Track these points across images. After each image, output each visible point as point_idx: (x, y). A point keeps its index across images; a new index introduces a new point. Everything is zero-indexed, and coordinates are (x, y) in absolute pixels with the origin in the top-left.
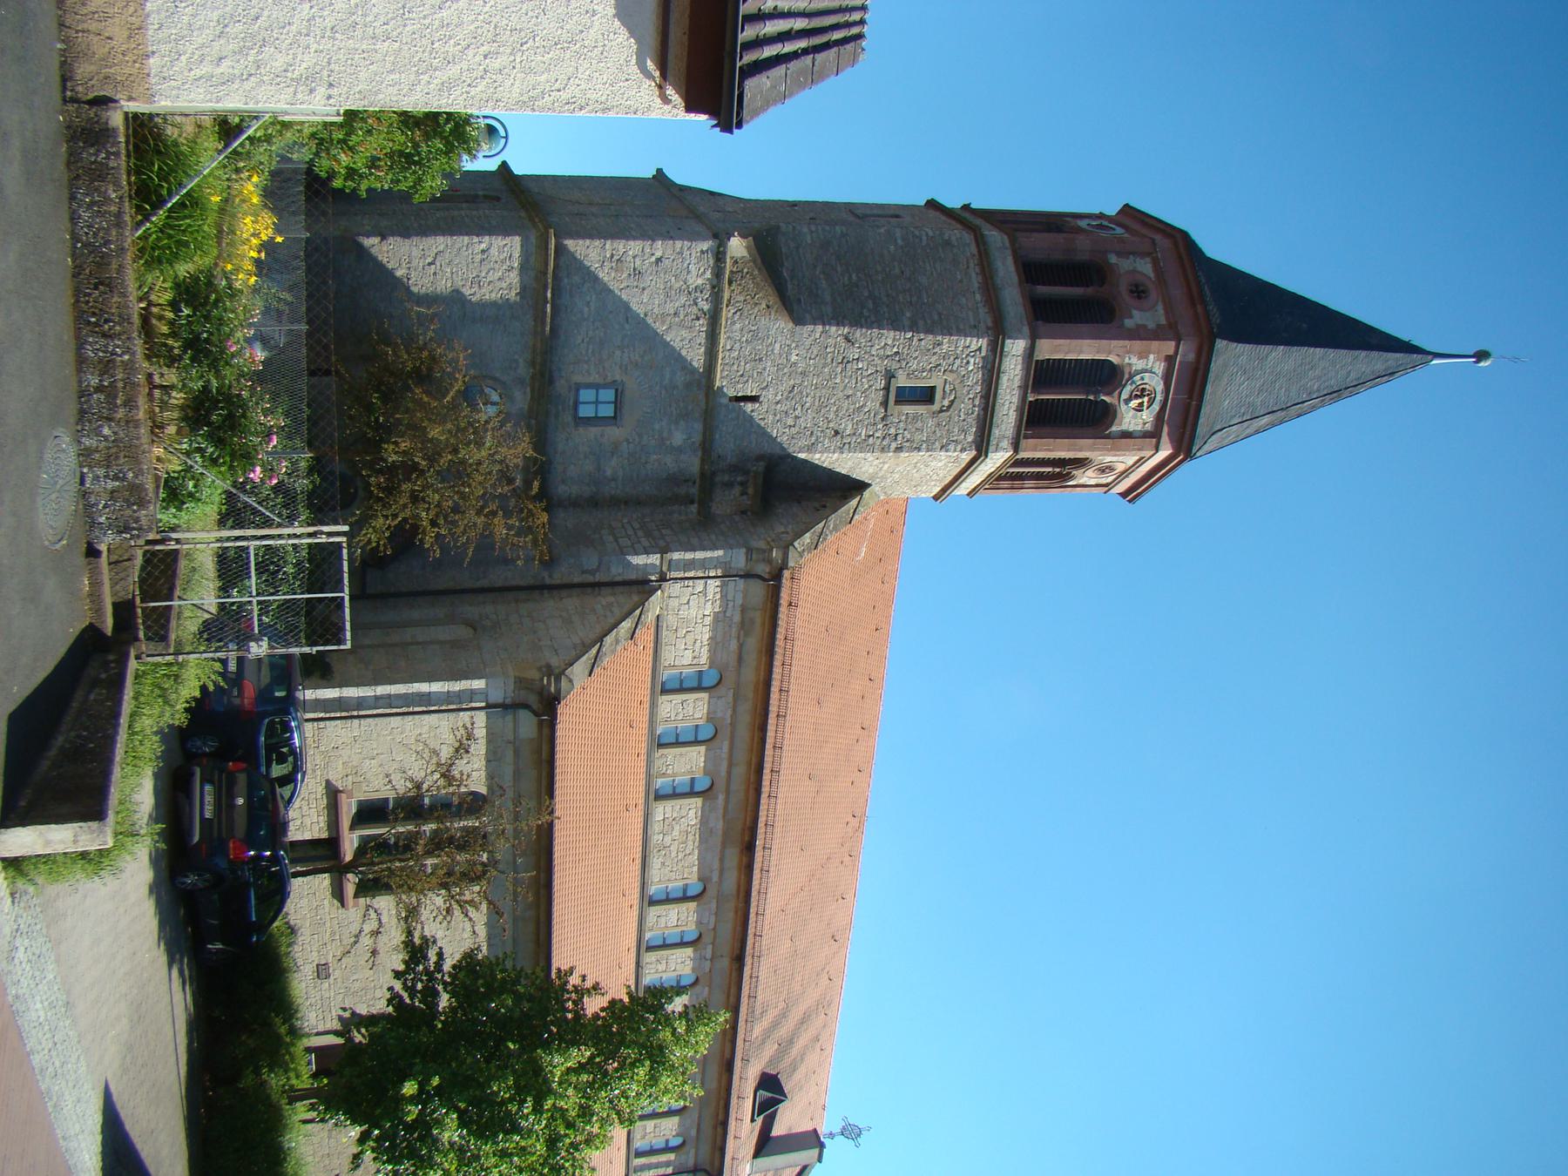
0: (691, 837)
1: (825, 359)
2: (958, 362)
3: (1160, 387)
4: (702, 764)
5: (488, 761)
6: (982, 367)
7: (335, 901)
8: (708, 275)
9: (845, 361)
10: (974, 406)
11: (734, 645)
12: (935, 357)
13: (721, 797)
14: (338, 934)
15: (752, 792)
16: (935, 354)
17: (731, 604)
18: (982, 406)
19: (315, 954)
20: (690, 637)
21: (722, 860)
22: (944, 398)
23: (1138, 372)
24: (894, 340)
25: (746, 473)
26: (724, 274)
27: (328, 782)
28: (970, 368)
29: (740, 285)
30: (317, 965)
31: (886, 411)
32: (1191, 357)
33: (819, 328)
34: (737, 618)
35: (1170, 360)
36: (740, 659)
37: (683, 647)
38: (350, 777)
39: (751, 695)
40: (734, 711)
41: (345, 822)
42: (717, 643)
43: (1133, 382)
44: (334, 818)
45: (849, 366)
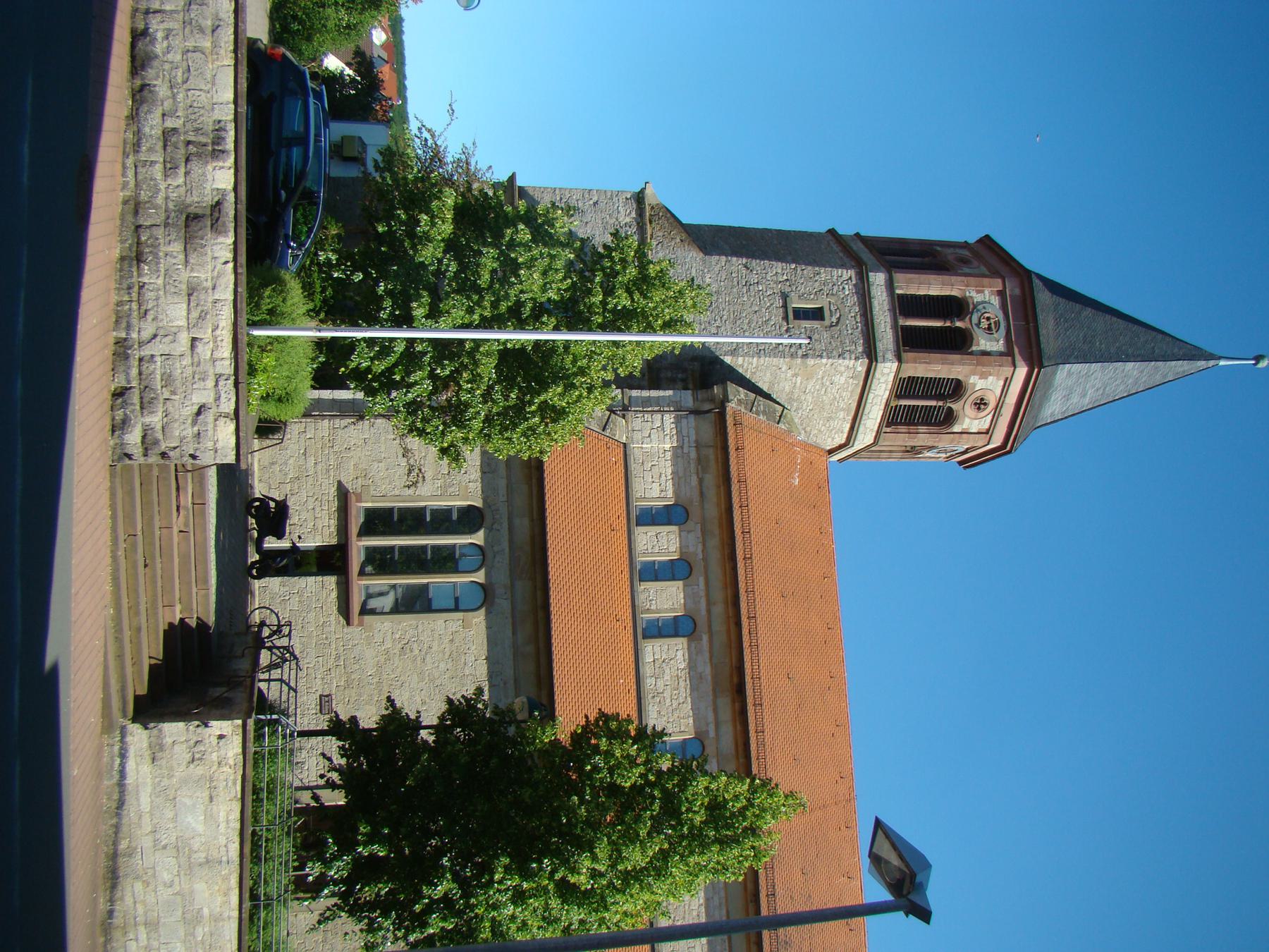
0: (682, 684)
1: (732, 281)
3: (1001, 317)
4: (682, 601)
5: (483, 473)
6: (856, 293)
7: (341, 618)
8: (634, 215)
9: (748, 284)
10: (857, 322)
11: (694, 481)
12: (817, 284)
13: (705, 638)
14: (342, 658)
15: (733, 627)
17: (686, 440)
18: (863, 323)
19: (319, 682)
20: (655, 470)
21: (715, 711)
22: (831, 316)
23: (979, 303)
24: (782, 269)
25: (685, 371)
27: (340, 483)
28: (847, 293)
29: (658, 224)
30: (321, 696)
31: (788, 324)
32: (1017, 291)
33: (723, 258)
34: (693, 455)
35: (1001, 294)
36: (702, 494)
37: (650, 480)
38: (360, 479)
39: (717, 531)
40: (704, 545)
41: (354, 529)
42: (679, 478)
43: (978, 310)
44: (344, 523)
45: (752, 287)
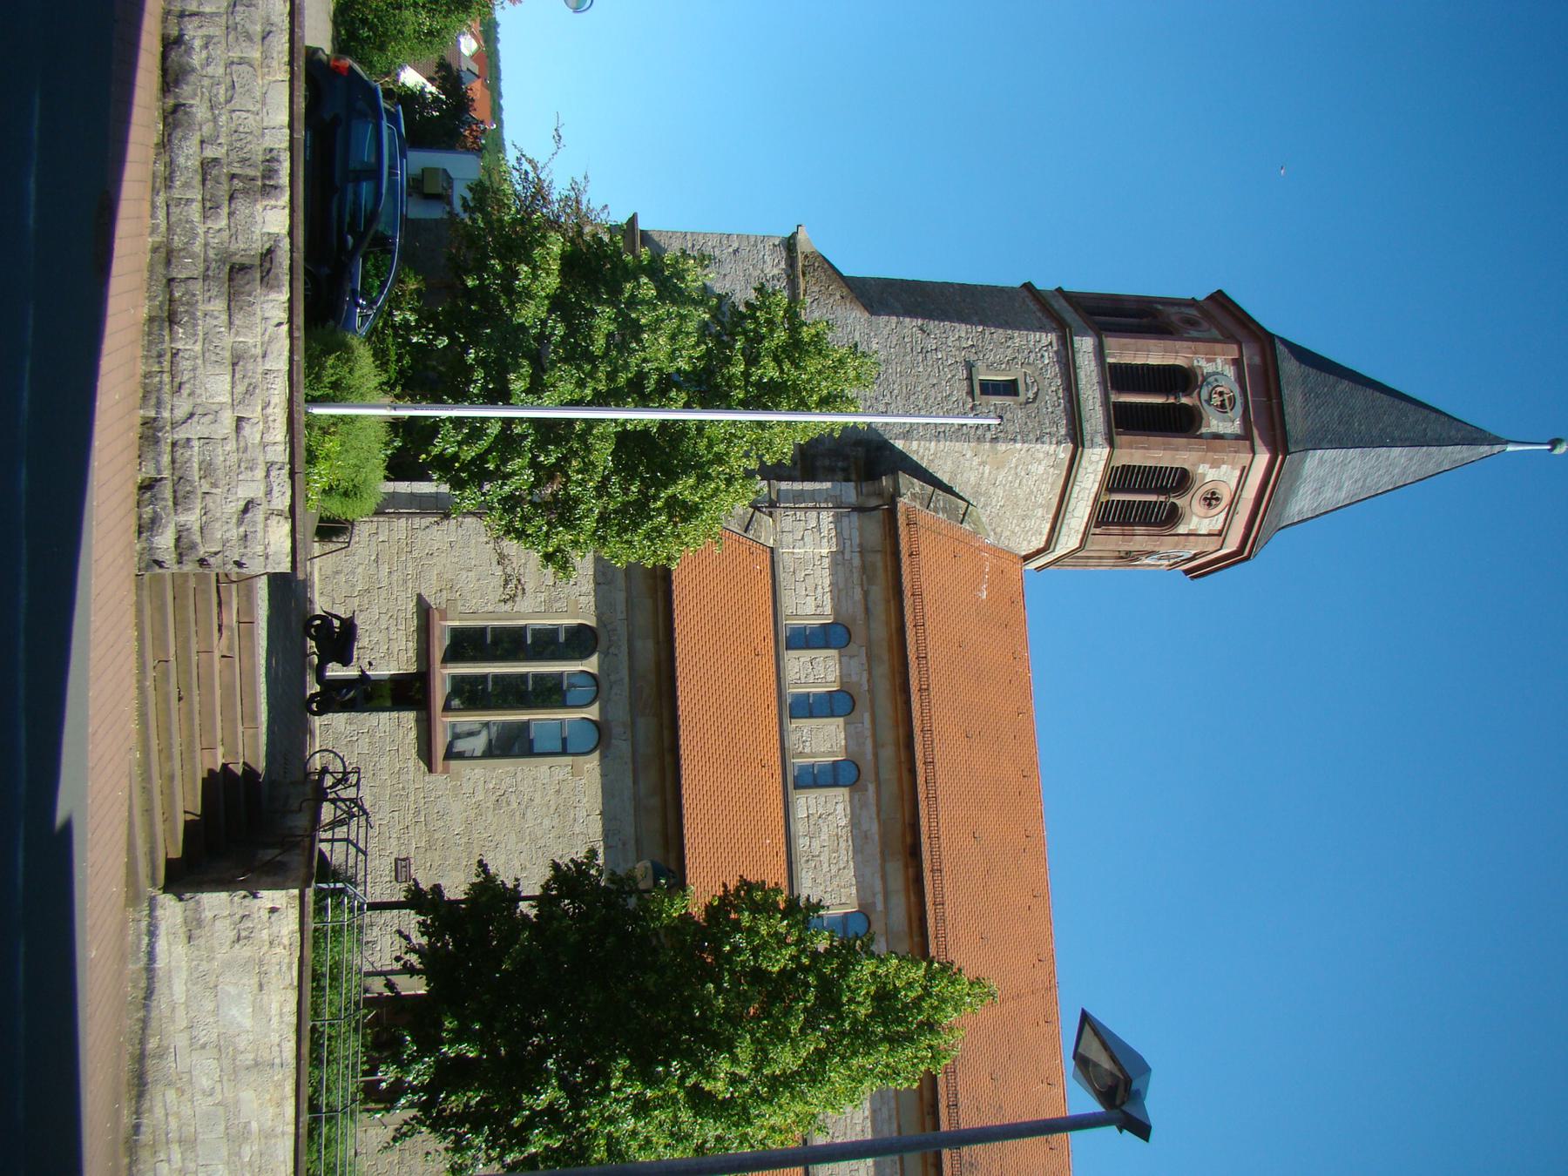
0: (843, 845)
1: (905, 348)
2: (1032, 356)
3: (1237, 391)
4: (843, 743)
5: (597, 584)
6: (1057, 361)
7: (421, 764)
8: (783, 265)
9: (924, 351)
10: (1059, 398)
11: (858, 594)
13: (871, 788)
14: (423, 813)
15: (905, 774)
16: (1008, 347)
17: (848, 543)
18: (1067, 399)
19: (394, 842)
20: (810, 580)
21: (884, 878)
22: (1027, 390)
24: (967, 332)
25: (846, 458)
26: (797, 262)
27: (420, 596)
28: (1046, 362)
29: (813, 277)
30: (396, 860)
31: (974, 400)
32: (1257, 360)
33: (894, 319)
34: (857, 561)
35: (1237, 363)
36: (867, 610)
37: (804, 593)
38: (445, 592)
39: (885, 656)
40: (870, 673)
41: (438, 653)
42: (839, 591)
43: (1208, 384)
44: (425, 646)
45: (929, 355)
